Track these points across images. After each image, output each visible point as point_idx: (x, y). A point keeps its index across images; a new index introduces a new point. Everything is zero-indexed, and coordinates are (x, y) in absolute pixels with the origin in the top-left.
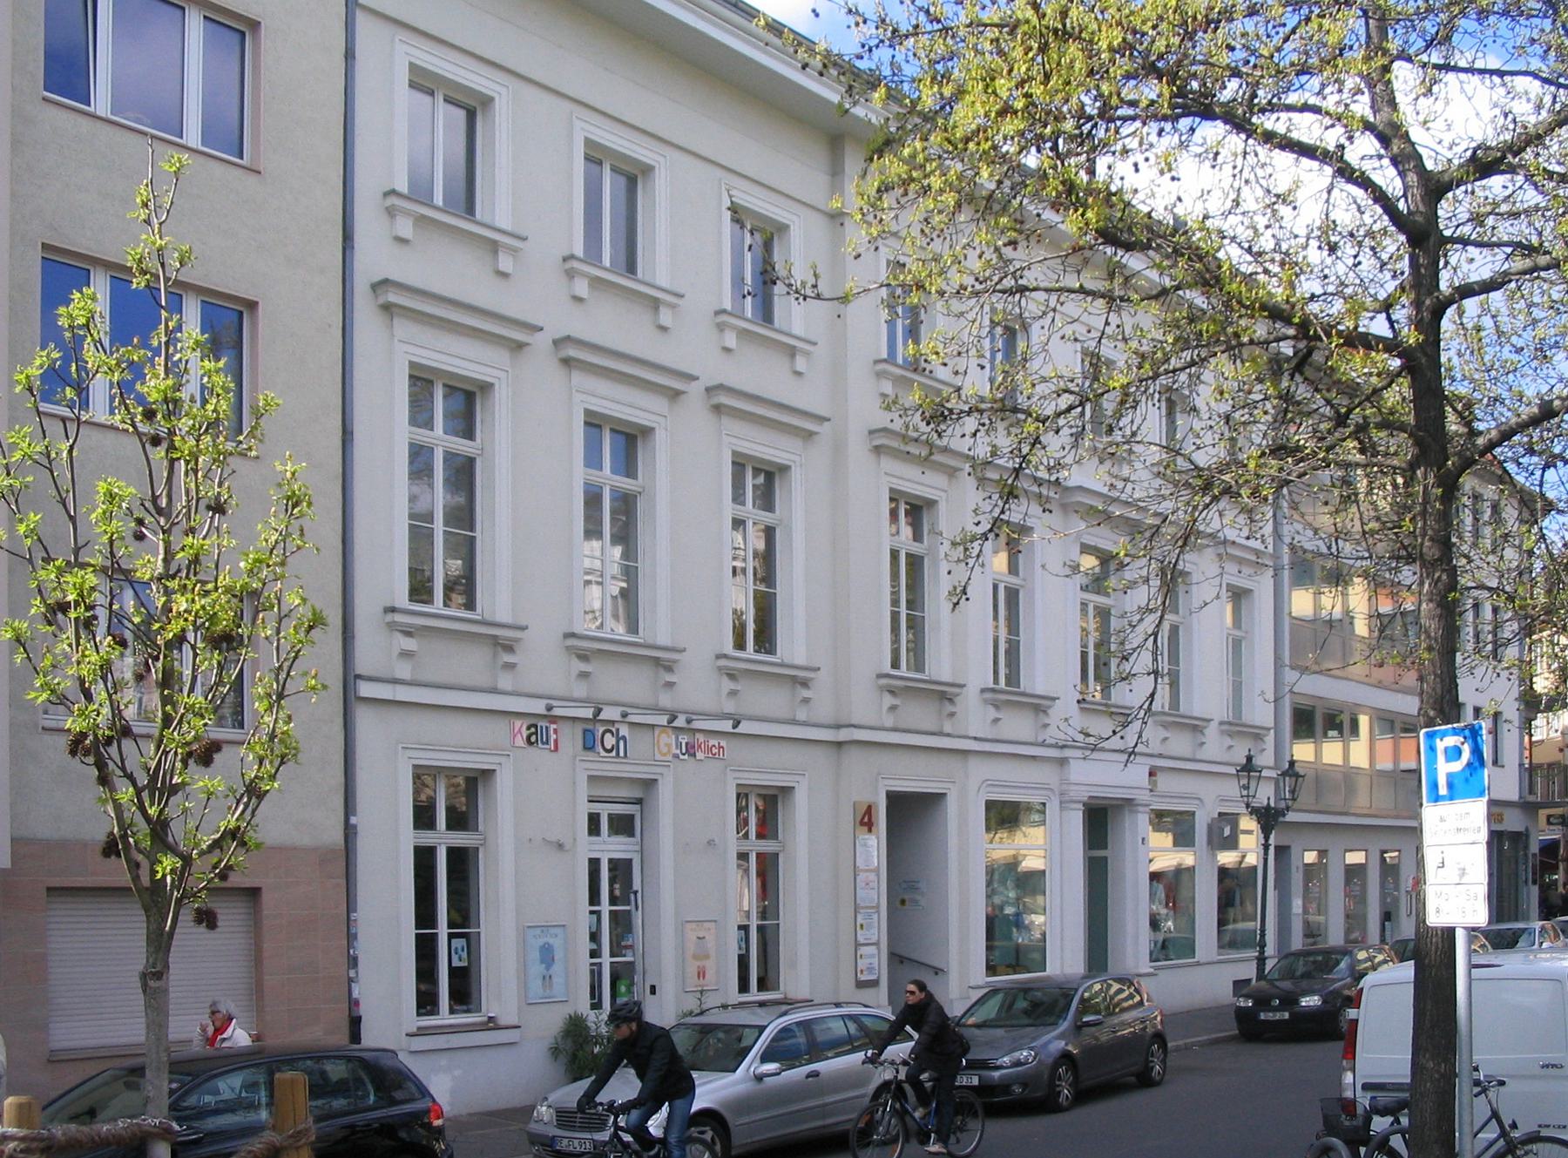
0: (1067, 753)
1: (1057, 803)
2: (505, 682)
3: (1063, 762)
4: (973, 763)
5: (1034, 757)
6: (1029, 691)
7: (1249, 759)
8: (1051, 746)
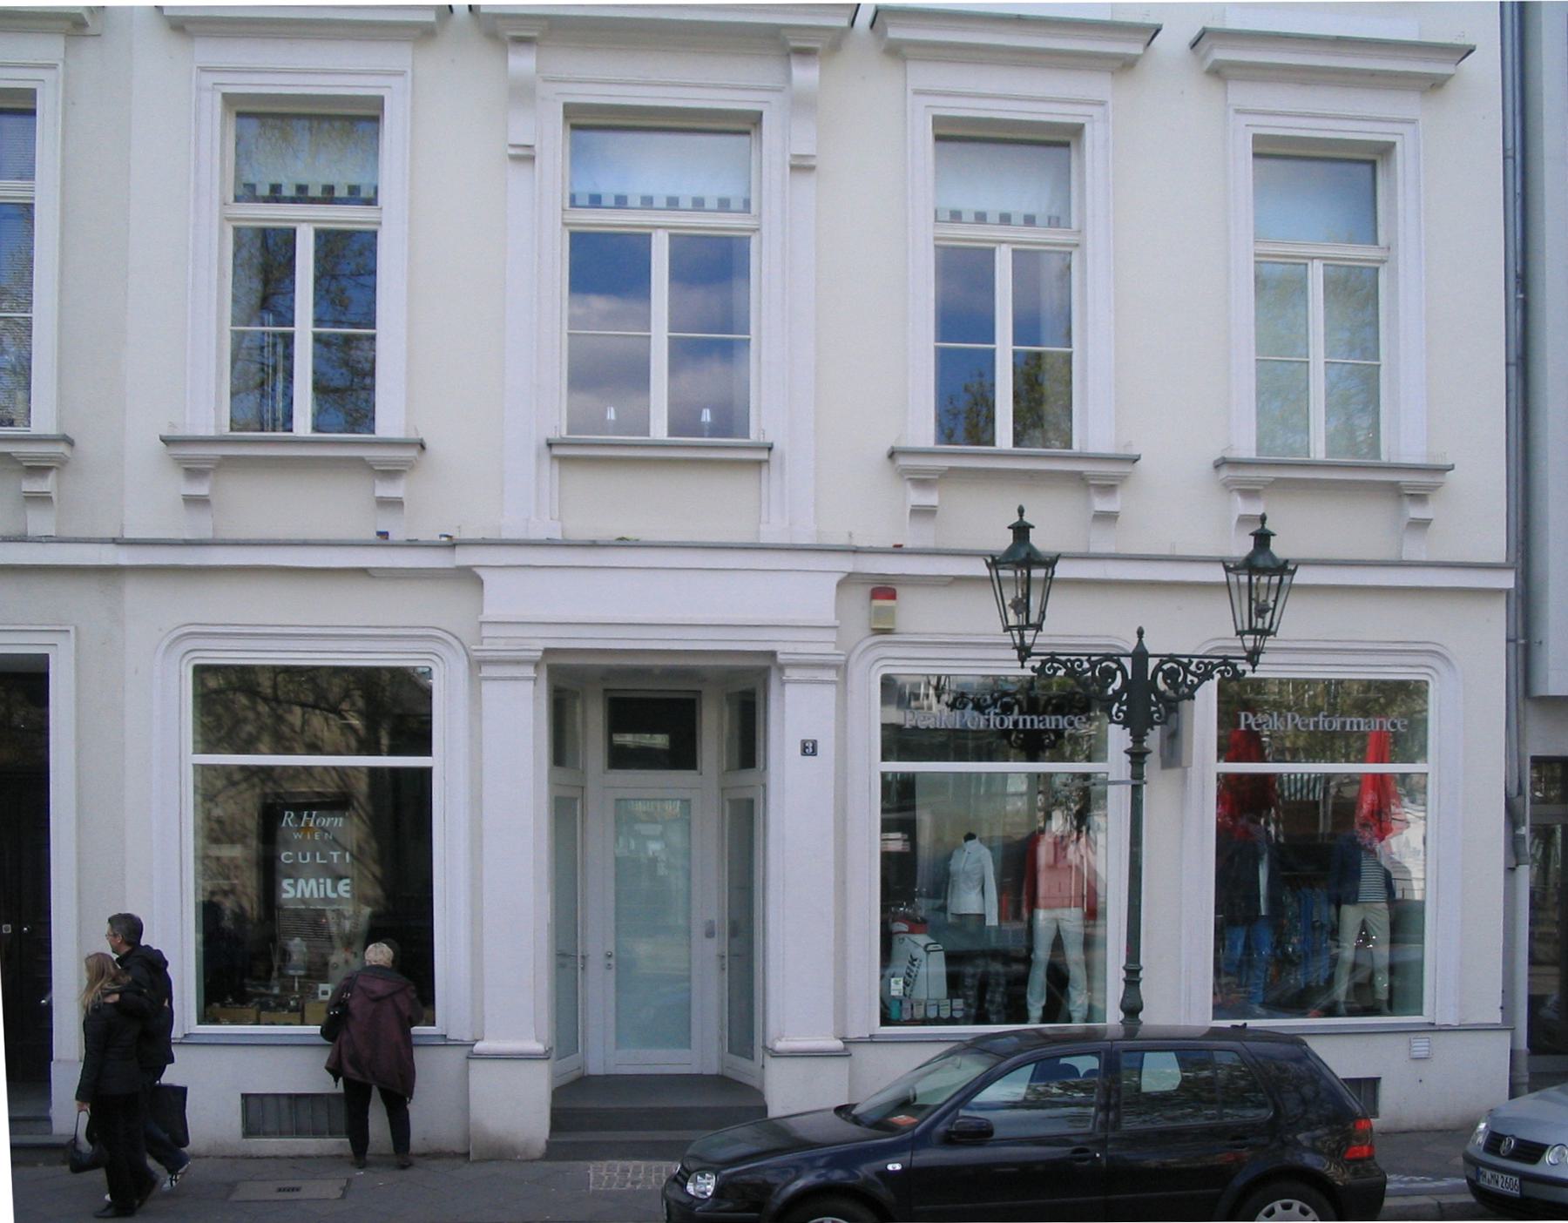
0: (463, 558)
1: (461, 667)
2: (40, 522)
3: (469, 577)
4: (135, 594)
5: (364, 572)
6: (1394, 460)
7: (1021, 531)
8: (412, 544)
